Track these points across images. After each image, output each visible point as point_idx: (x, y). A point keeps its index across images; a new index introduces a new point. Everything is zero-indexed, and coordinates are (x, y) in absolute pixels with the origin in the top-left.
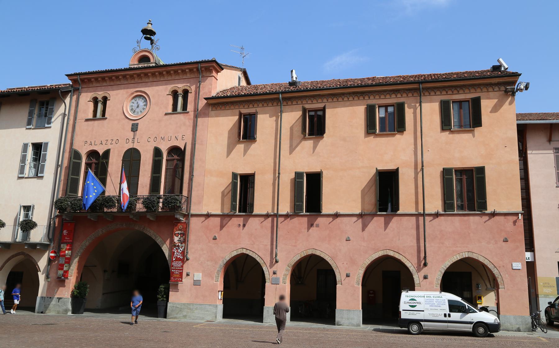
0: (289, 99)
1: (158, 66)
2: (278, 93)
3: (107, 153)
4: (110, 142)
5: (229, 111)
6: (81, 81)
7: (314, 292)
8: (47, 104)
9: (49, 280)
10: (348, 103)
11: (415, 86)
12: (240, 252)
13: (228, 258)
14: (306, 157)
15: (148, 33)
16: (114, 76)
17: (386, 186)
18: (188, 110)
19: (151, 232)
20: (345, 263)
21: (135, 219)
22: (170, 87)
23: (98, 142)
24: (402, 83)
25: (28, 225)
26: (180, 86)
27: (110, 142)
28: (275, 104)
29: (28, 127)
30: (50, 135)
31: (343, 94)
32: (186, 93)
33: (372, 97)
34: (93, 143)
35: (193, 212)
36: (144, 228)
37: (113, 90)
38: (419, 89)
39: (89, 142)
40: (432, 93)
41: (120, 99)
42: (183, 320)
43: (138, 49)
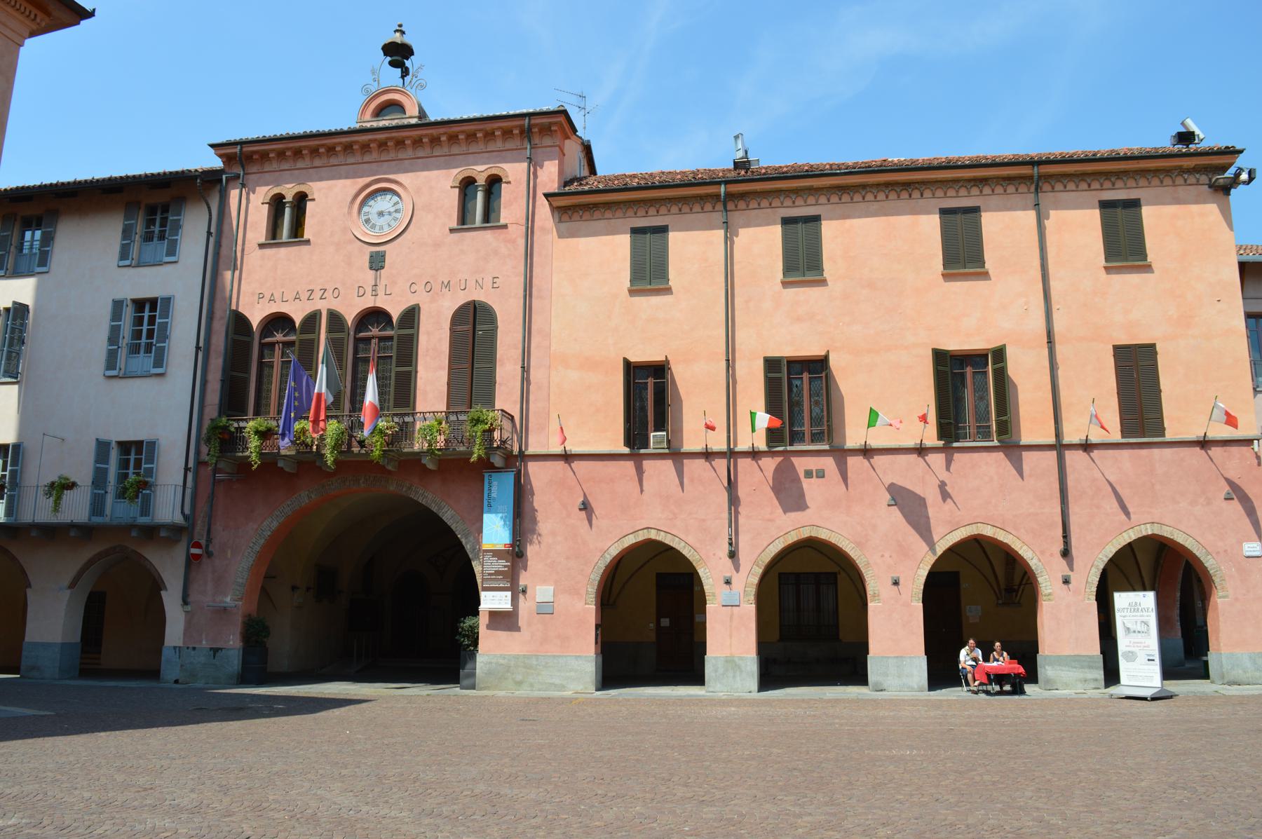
0: (742, 196)
1: (424, 123)
2: (719, 183)
3: (411, 316)
4: (318, 294)
5: (602, 223)
6: (244, 158)
7: (813, 623)
8: (165, 209)
9: (189, 608)
10: (875, 206)
11: (1025, 171)
12: (641, 537)
13: (614, 551)
14: (786, 323)
15: (398, 53)
16: (323, 145)
17: (648, 395)
18: (306, 237)
19: (430, 497)
20: (887, 555)
21: (390, 468)
22: (452, 175)
23: (289, 296)
24: (940, 167)
25: (139, 488)
26: (481, 171)
27: (318, 294)
28: (708, 207)
29: (122, 263)
30: (177, 279)
31: (864, 186)
32: (494, 182)
33: (663, 210)
34: (277, 296)
35: (531, 450)
36: (409, 488)
37: (321, 179)
38: (1030, 178)
39: (268, 296)
40: (1059, 186)
41: (330, 197)
42: (523, 692)
43: (374, 88)
